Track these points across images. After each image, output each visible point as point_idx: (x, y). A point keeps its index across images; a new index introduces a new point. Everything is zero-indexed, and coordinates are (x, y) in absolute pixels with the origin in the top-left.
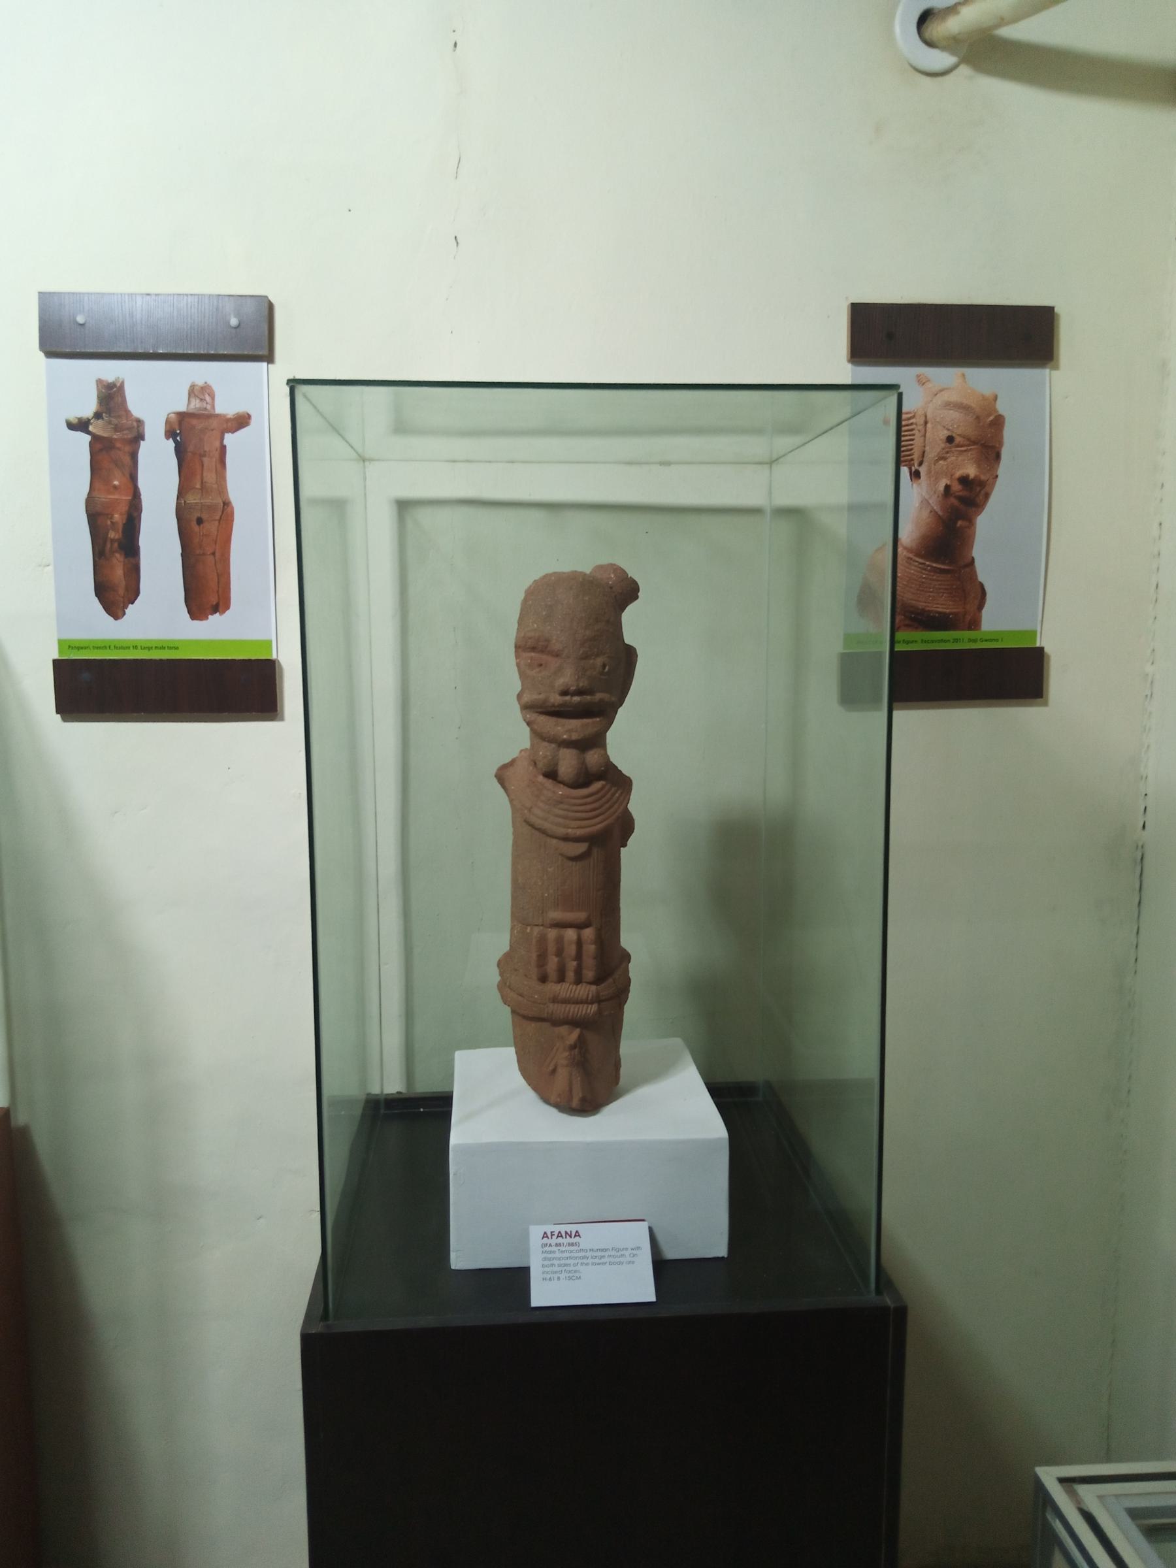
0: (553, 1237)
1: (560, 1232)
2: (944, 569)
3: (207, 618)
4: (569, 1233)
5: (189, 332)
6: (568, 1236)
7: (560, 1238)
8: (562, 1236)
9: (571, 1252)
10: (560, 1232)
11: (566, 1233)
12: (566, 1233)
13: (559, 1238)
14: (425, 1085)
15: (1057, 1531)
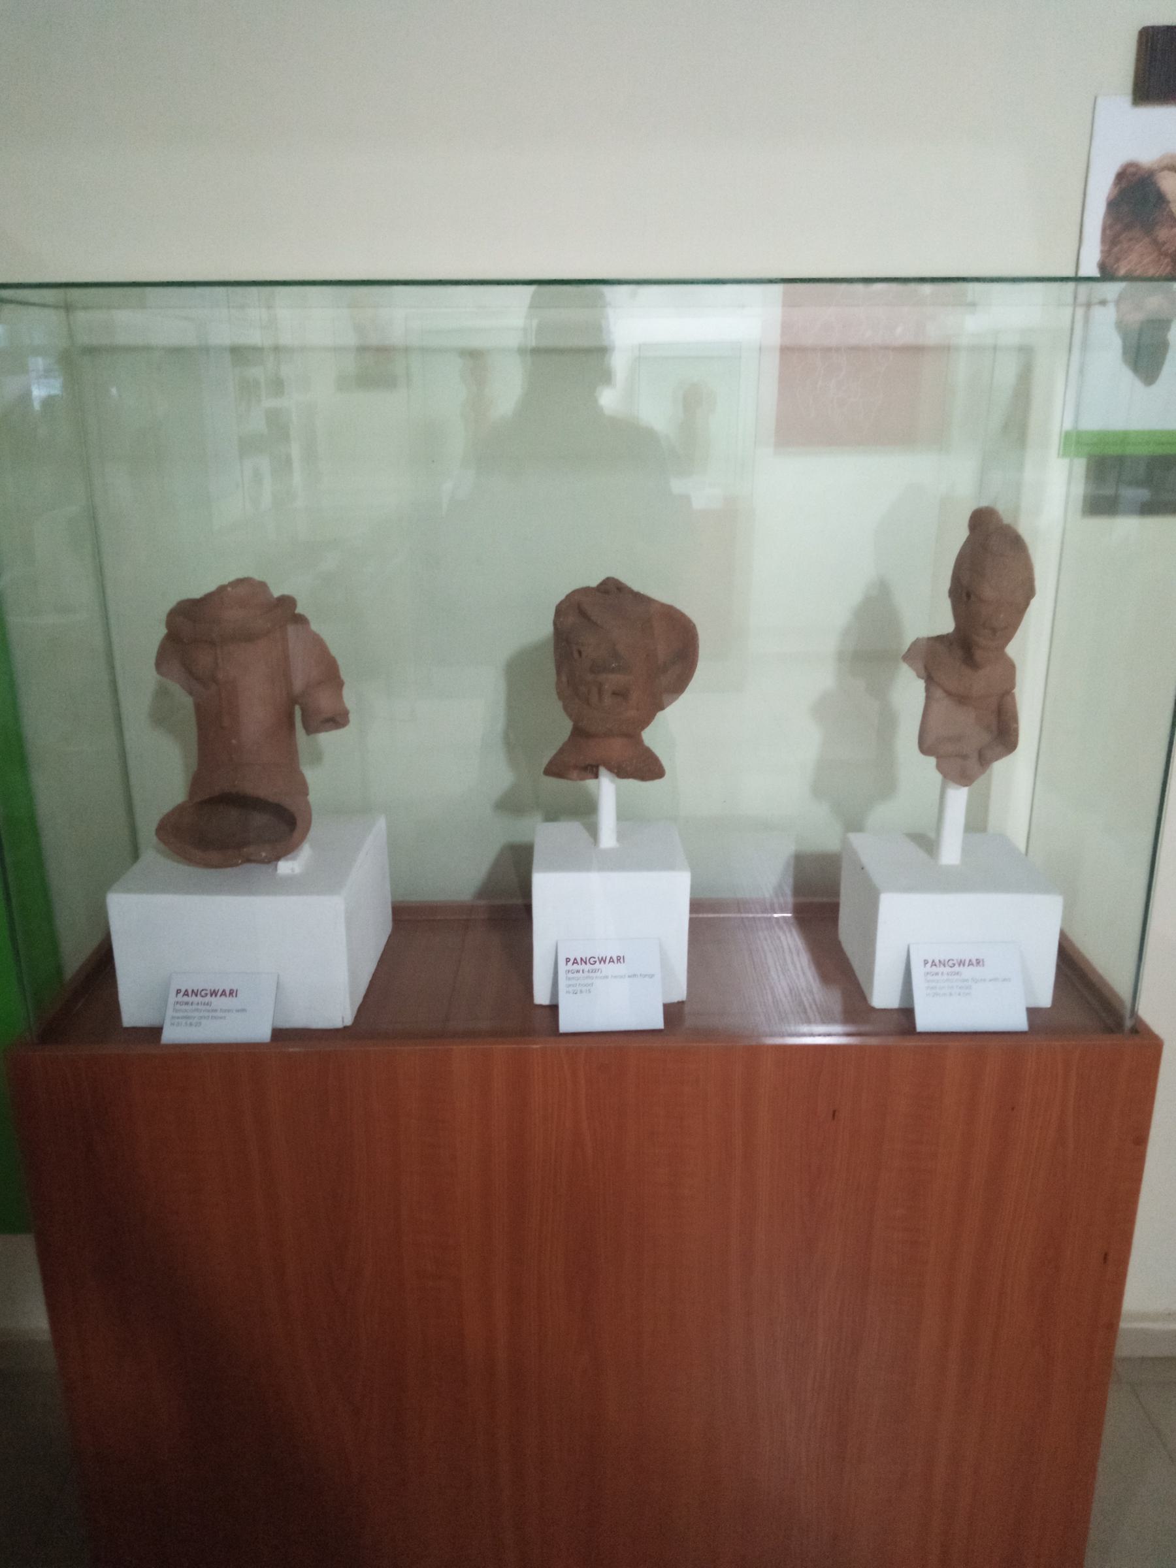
0: (569, 963)
1: (575, 959)
2: (708, 912)
3: (280, 1035)
4: (196, 991)
5: (822, 999)
6: (194, 995)
7: (186, 997)
8: (577, 963)
9: (186, 1011)
10: (575, 959)
11: (582, 959)
12: (582, 959)
13: (575, 965)
14: (554, 1003)
15: (813, 968)
